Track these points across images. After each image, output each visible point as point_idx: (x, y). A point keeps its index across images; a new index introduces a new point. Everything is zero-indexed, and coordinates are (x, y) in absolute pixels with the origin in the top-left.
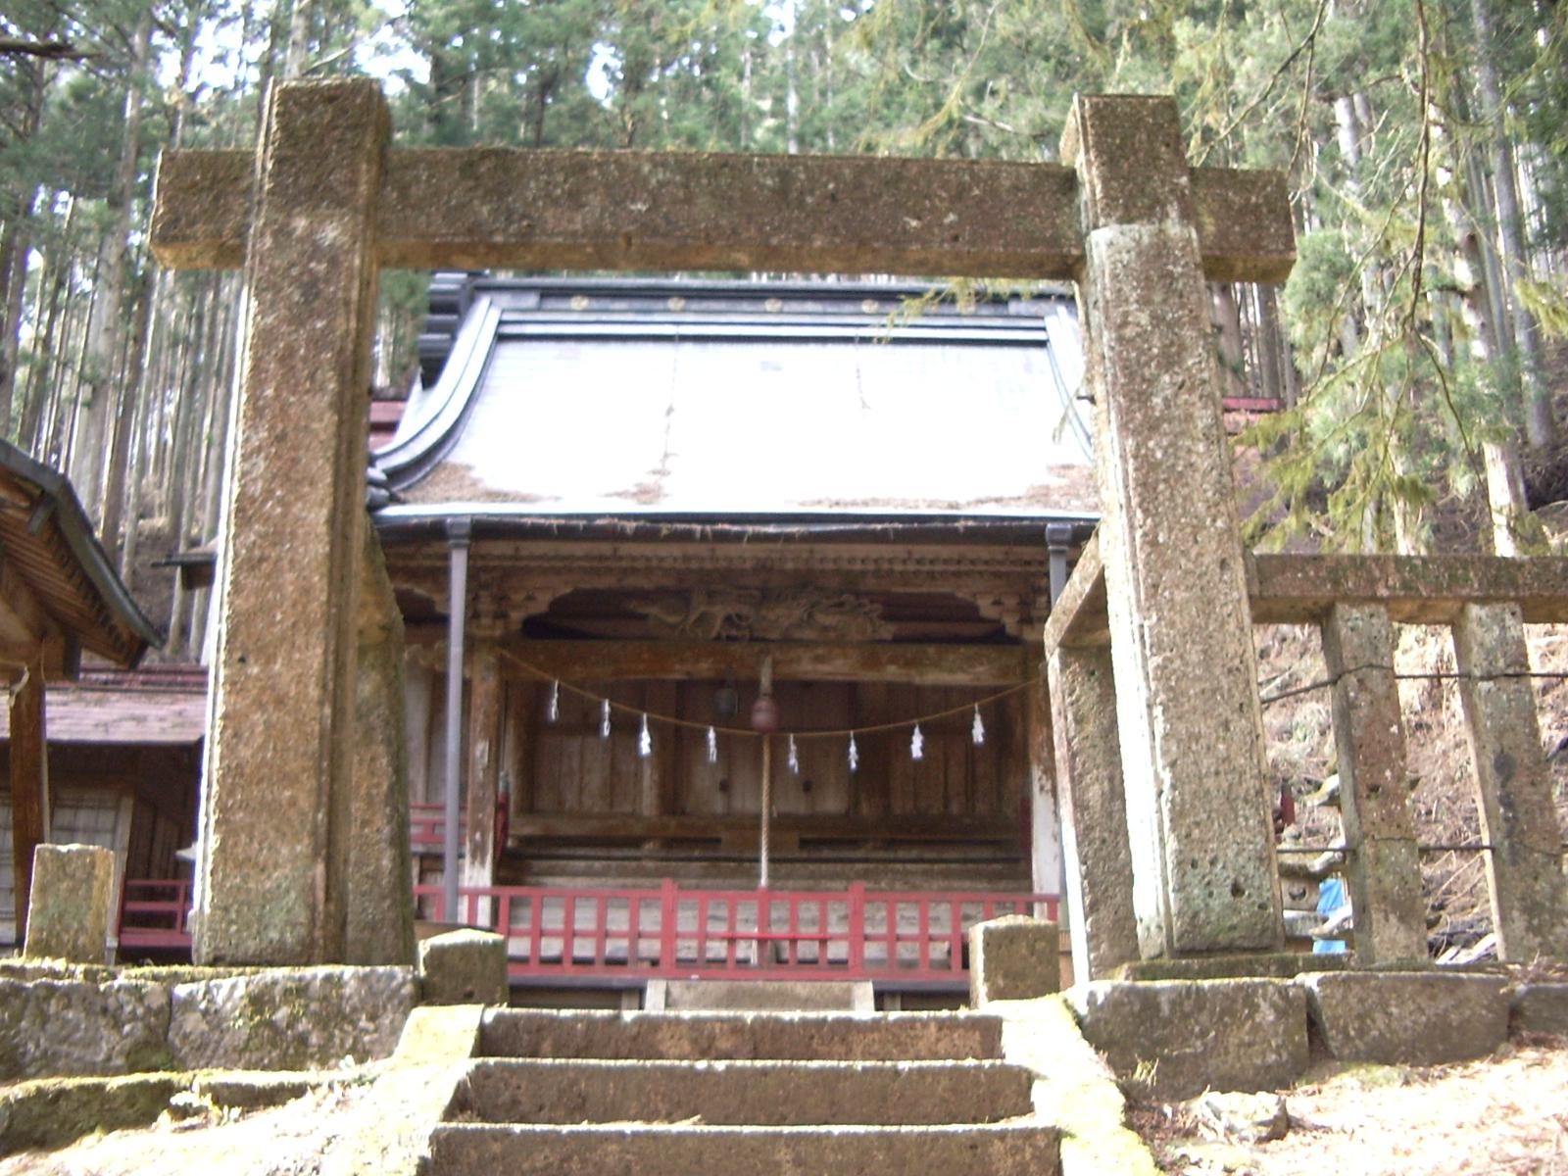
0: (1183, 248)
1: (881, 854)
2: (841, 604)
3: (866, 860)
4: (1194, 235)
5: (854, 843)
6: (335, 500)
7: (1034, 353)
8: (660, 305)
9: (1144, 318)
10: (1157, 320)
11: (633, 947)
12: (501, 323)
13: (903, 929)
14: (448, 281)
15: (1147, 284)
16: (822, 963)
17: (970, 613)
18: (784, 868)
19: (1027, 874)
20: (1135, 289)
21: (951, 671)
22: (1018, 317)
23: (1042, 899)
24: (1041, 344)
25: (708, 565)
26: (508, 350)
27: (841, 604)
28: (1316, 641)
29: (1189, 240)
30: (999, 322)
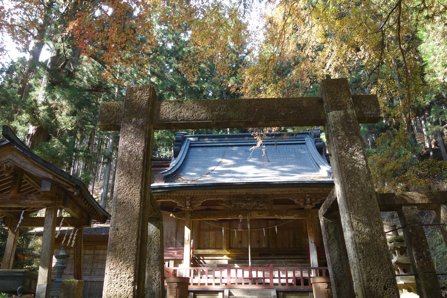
0: (352, 116)
1: (276, 257)
2: (264, 202)
3: (272, 259)
4: (355, 112)
5: (269, 255)
6: (142, 187)
7: (303, 145)
8: (223, 139)
9: (343, 134)
10: (346, 134)
11: (221, 281)
12: (190, 144)
13: (282, 276)
14: (15, 31)
15: (343, 125)
16: (264, 284)
17: (292, 203)
18: (254, 261)
19: (310, 262)
20: (340, 127)
21: (289, 216)
22: (299, 138)
23: (313, 268)
24: (304, 144)
25: (235, 194)
26: (192, 150)
27: (264, 202)
28: (396, 214)
29: (354, 114)
30: (295, 140)
